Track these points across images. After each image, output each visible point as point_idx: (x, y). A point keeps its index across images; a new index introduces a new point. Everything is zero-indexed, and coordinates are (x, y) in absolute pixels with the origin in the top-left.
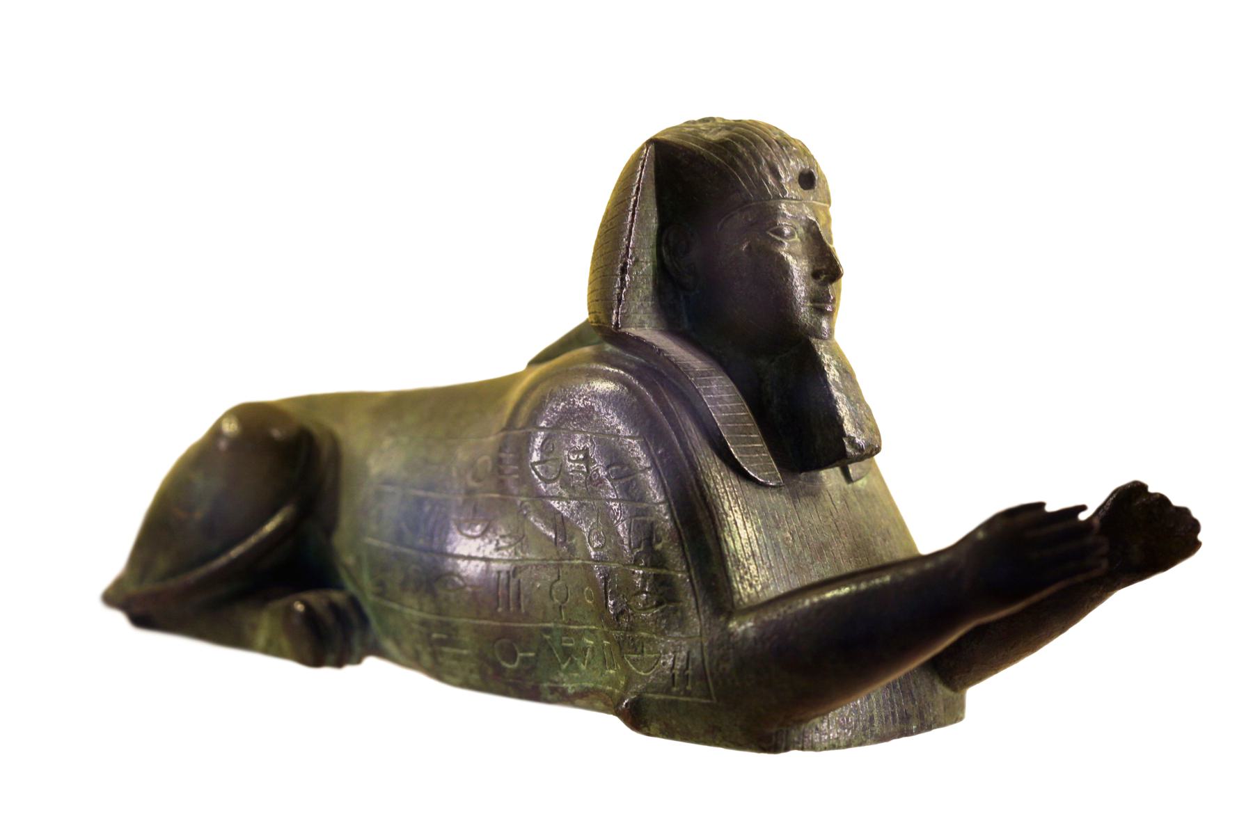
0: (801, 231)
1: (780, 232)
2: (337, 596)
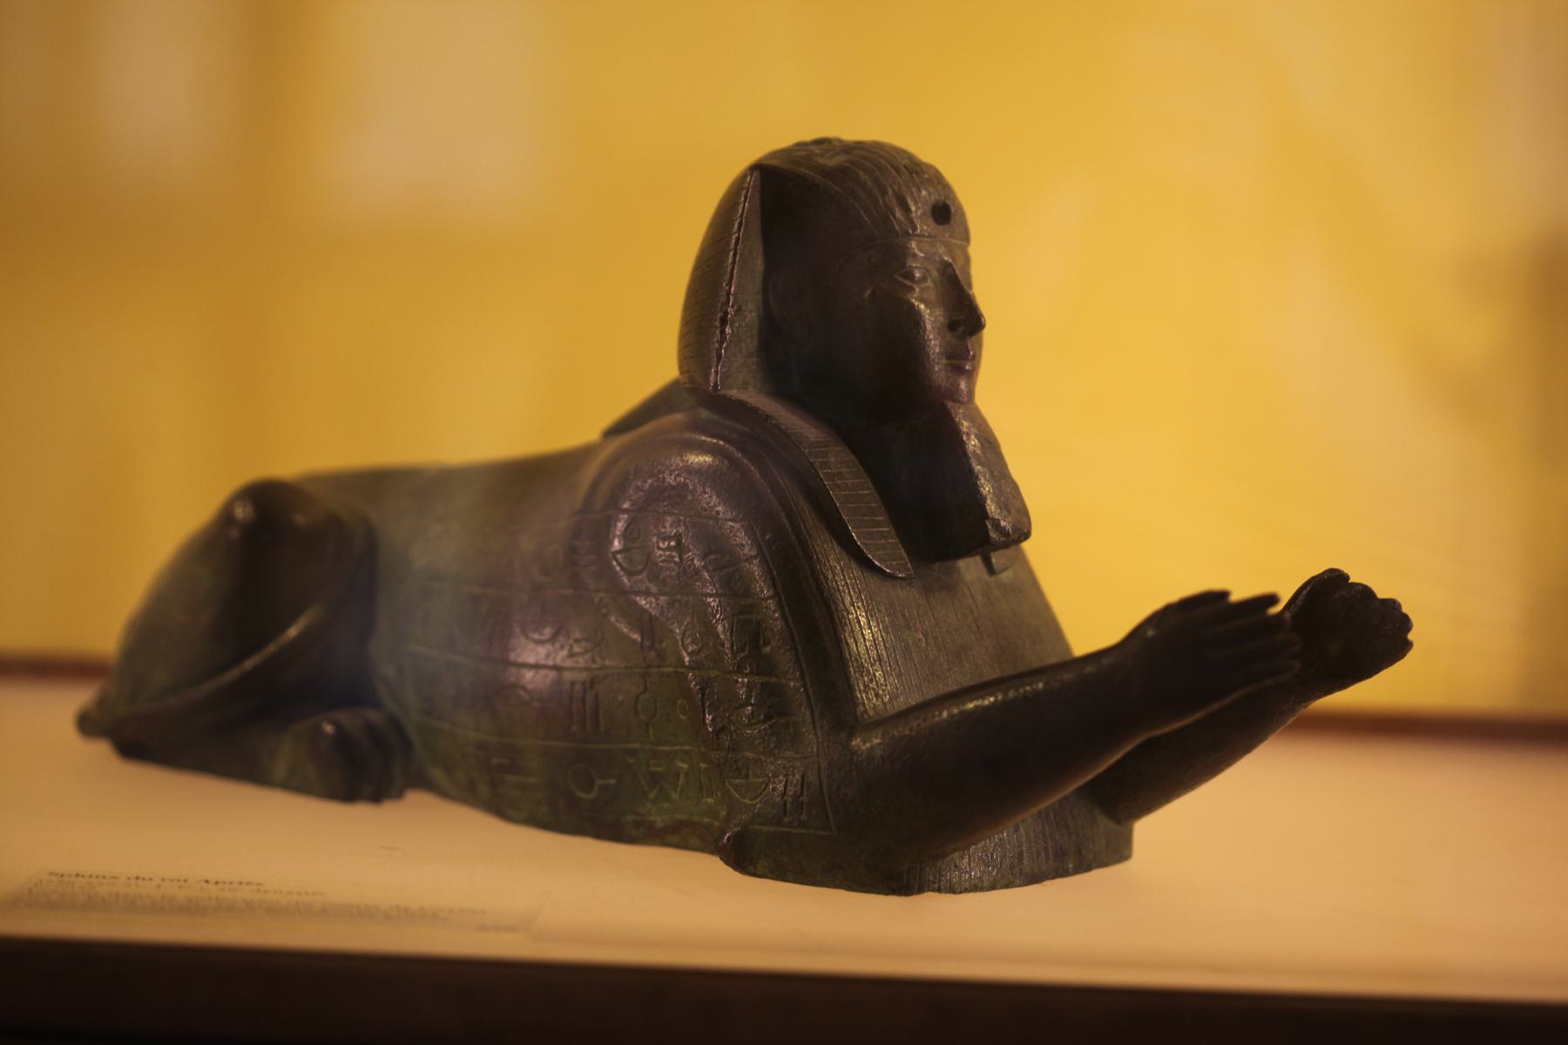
0: (935, 274)
2: (373, 715)
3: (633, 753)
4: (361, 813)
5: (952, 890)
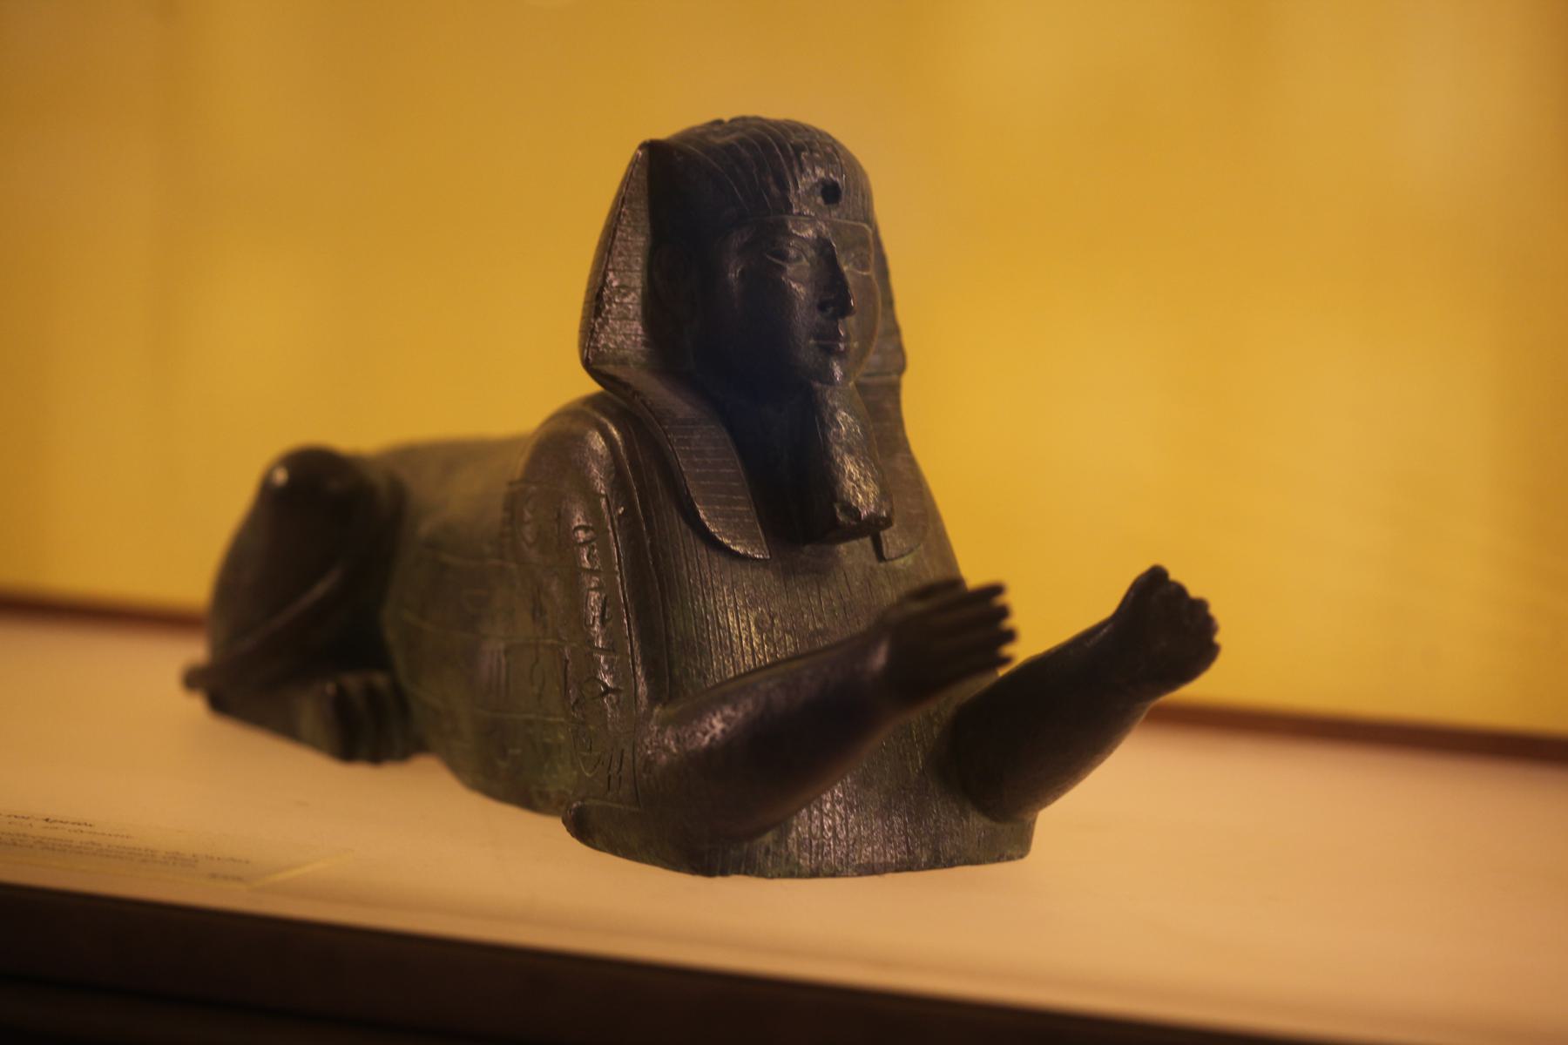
0: (811, 253)
1: (783, 256)
2: (380, 680)
3: (529, 723)
4: (359, 775)
5: (794, 872)
